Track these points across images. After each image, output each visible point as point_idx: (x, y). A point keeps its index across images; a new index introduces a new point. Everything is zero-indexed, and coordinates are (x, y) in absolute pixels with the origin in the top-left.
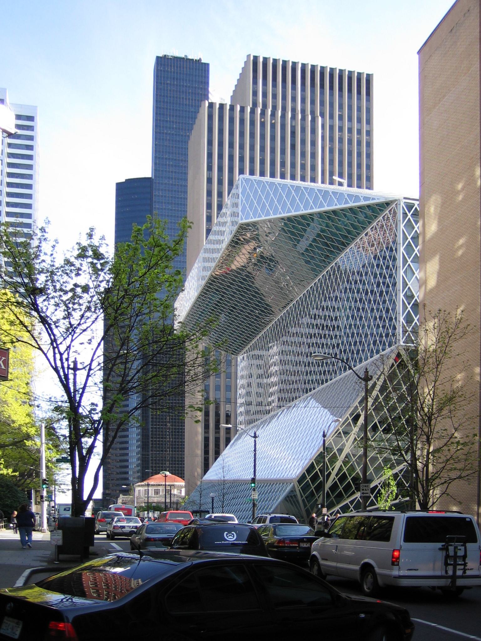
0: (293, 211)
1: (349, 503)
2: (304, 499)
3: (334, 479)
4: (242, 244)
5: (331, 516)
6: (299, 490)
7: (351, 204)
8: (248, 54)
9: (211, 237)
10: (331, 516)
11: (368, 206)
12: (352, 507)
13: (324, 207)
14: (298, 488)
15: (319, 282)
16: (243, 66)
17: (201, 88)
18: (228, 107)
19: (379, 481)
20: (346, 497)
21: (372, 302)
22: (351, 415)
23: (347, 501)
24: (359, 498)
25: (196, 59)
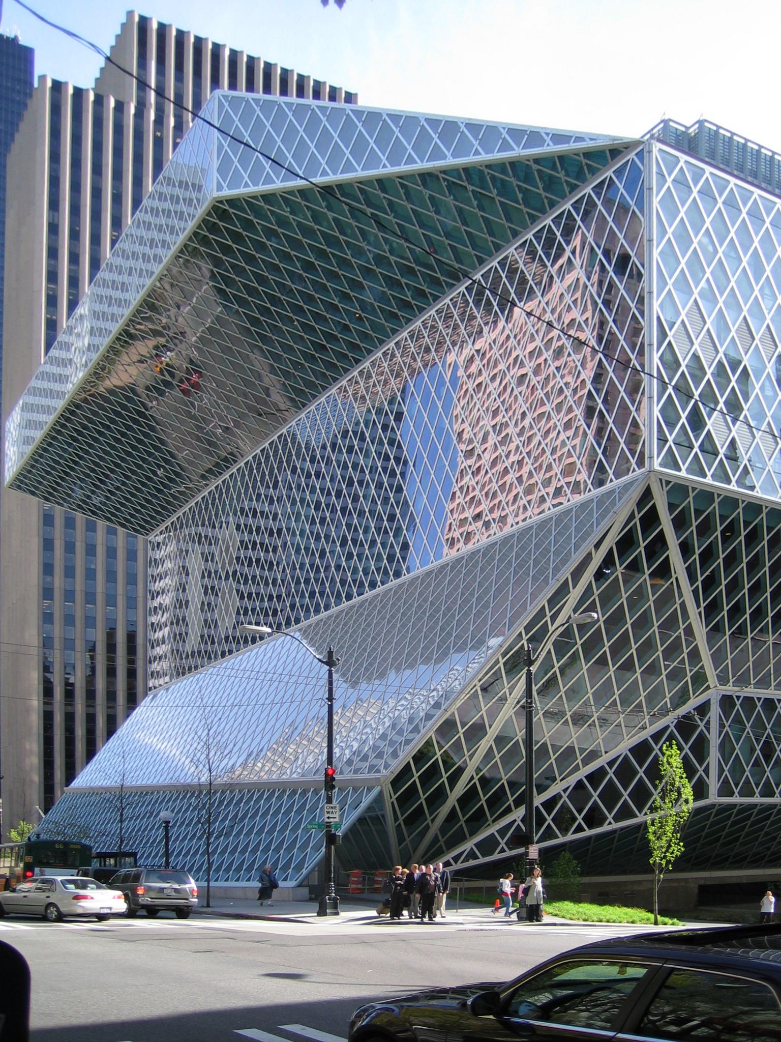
0: (359, 169)
1: (496, 834)
2: (400, 824)
3: (472, 778)
4: (143, 338)
5: (456, 863)
6: (392, 803)
7: (518, 152)
8: (130, 9)
9: (54, 352)
10: (456, 863)
11: (562, 158)
12: (503, 843)
13: (444, 157)
14: (390, 798)
15: (203, 501)
16: (119, 32)
17: (19, 92)
18: (92, 97)
19: (564, 784)
20: (490, 820)
21: (298, 533)
22: (528, 629)
23: (493, 829)
24: (519, 822)
25: (9, 35)
